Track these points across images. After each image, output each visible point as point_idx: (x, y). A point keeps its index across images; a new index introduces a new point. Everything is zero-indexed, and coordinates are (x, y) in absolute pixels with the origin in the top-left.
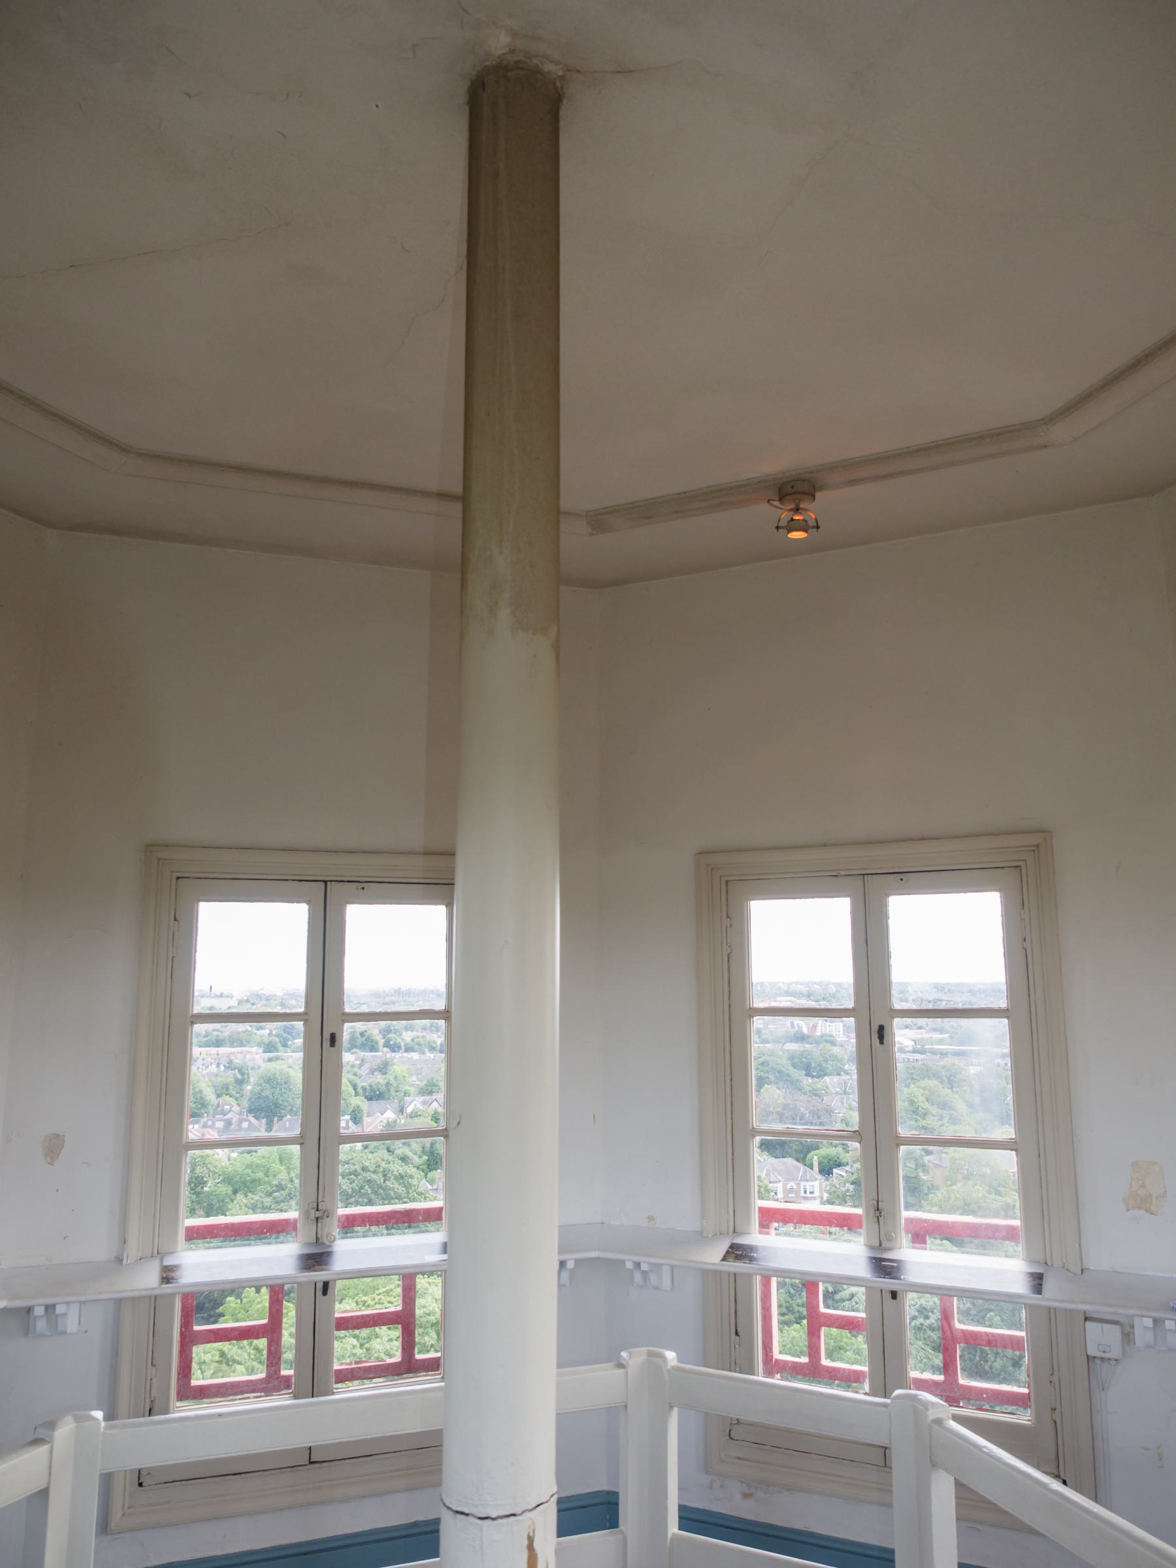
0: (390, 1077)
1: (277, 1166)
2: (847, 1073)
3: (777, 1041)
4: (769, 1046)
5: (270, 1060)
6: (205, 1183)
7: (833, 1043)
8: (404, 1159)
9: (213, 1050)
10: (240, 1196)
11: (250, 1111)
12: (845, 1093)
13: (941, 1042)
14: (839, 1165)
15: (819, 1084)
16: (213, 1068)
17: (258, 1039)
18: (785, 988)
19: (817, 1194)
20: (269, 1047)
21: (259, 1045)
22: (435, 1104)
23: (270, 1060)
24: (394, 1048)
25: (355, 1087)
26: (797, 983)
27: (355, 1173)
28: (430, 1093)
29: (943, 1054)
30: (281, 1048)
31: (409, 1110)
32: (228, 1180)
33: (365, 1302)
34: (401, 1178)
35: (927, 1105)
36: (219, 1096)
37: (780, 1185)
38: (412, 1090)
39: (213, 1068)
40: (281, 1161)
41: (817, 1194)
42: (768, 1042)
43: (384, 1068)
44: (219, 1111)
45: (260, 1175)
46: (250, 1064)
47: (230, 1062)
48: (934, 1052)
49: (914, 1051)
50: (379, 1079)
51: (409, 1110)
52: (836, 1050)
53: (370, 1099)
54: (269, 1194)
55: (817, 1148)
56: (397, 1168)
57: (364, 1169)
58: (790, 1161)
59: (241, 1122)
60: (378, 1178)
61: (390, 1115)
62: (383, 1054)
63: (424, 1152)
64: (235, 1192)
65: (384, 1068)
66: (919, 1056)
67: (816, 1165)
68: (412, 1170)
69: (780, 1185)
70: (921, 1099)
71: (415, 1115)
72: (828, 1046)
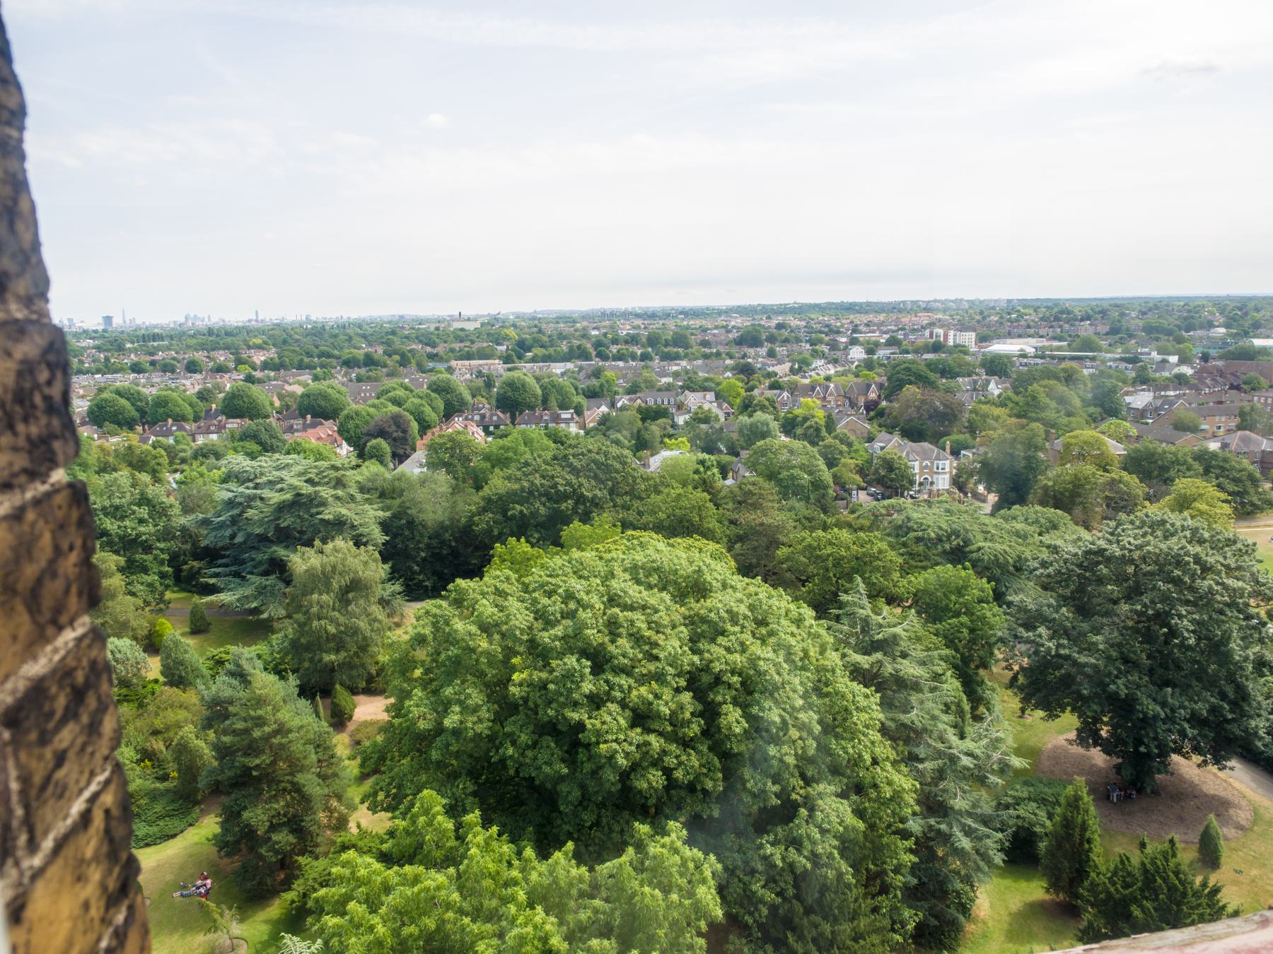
0: (602, 380)
1: (522, 448)
2: (977, 374)
3: (916, 352)
4: (910, 356)
5: (509, 370)
6: (471, 460)
7: (966, 353)
8: (617, 442)
9: (467, 363)
10: (497, 470)
11: (498, 407)
12: (975, 389)
13: (1059, 349)
14: (966, 448)
15: (952, 383)
16: (468, 376)
17: (499, 353)
18: (923, 306)
19: (947, 470)
20: (507, 359)
21: (500, 358)
22: (639, 401)
23: (509, 370)
24: (604, 357)
25: (576, 389)
26: (935, 301)
27: (583, 454)
28: (635, 392)
29: (1063, 359)
30: (515, 358)
31: (619, 405)
32: (487, 458)
33: (1195, 531)
34: (617, 458)
35: (1048, 400)
36: (474, 396)
37: (917, 464)
38: (620, 390)
39: (468, 376)
40: (525, 444)
41: (947, 470)
42: (908, 352)
43: (597, 373)
44: (475, 408)
45: (511, 454)
46: (495, 373)
47: (480, 372)
48: (1053, 357)
49: (1036, 357)
50: (595, 382)
51: (619, 405)
52: (968, 358)
53: (588, 397)
54: (519, 469)
55: (949, 434)
56: (615, 450)
57: (590, 451)
58: (926, 445)
59: (491, 416)
60: (601, 458)
61: (604, 409)
62: (596, 362)
63: (632, 437)
64: (493, 467)
65: (597, 373)
66: (1039, 361)
67: (948, 448)
68: (626, 452)
69: (917, 464)
70: (644, 626)
71: (623, 408)
72: (962, 356)
